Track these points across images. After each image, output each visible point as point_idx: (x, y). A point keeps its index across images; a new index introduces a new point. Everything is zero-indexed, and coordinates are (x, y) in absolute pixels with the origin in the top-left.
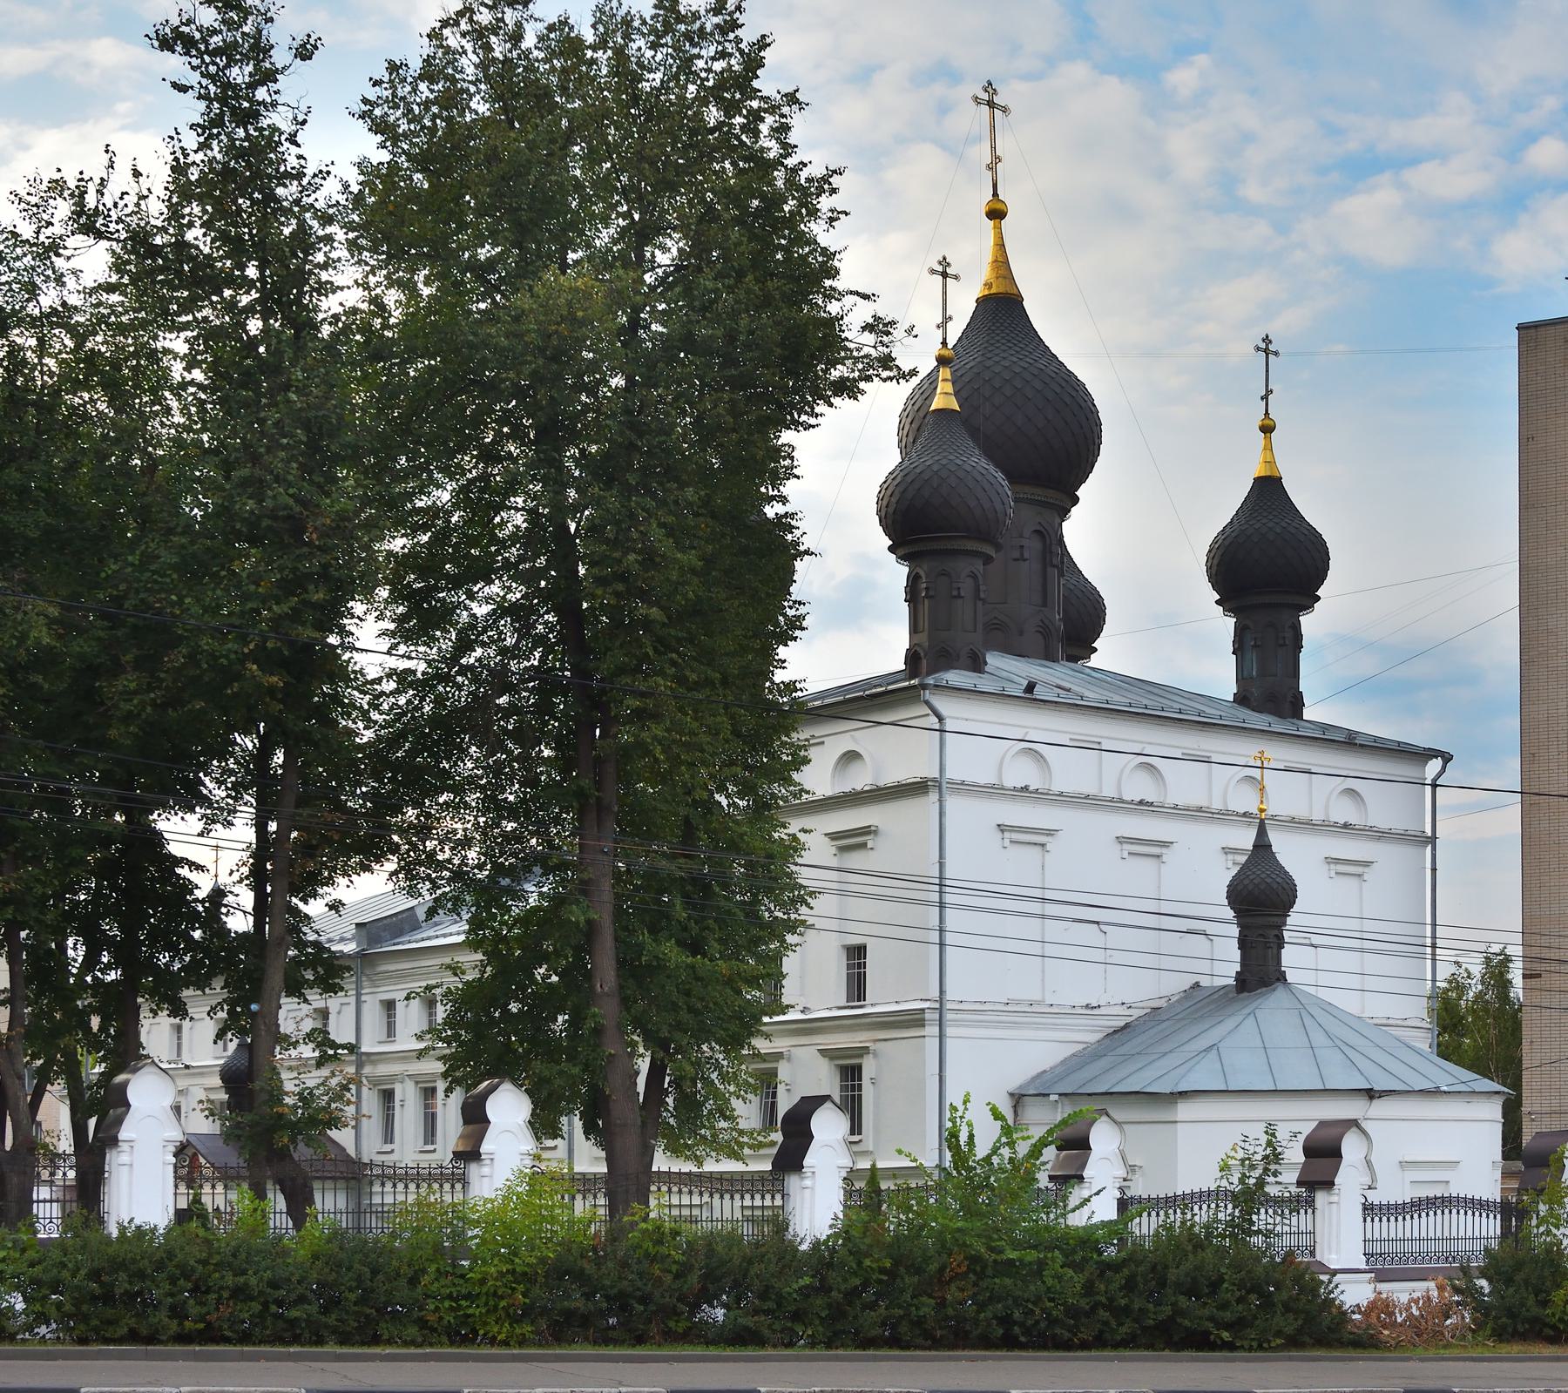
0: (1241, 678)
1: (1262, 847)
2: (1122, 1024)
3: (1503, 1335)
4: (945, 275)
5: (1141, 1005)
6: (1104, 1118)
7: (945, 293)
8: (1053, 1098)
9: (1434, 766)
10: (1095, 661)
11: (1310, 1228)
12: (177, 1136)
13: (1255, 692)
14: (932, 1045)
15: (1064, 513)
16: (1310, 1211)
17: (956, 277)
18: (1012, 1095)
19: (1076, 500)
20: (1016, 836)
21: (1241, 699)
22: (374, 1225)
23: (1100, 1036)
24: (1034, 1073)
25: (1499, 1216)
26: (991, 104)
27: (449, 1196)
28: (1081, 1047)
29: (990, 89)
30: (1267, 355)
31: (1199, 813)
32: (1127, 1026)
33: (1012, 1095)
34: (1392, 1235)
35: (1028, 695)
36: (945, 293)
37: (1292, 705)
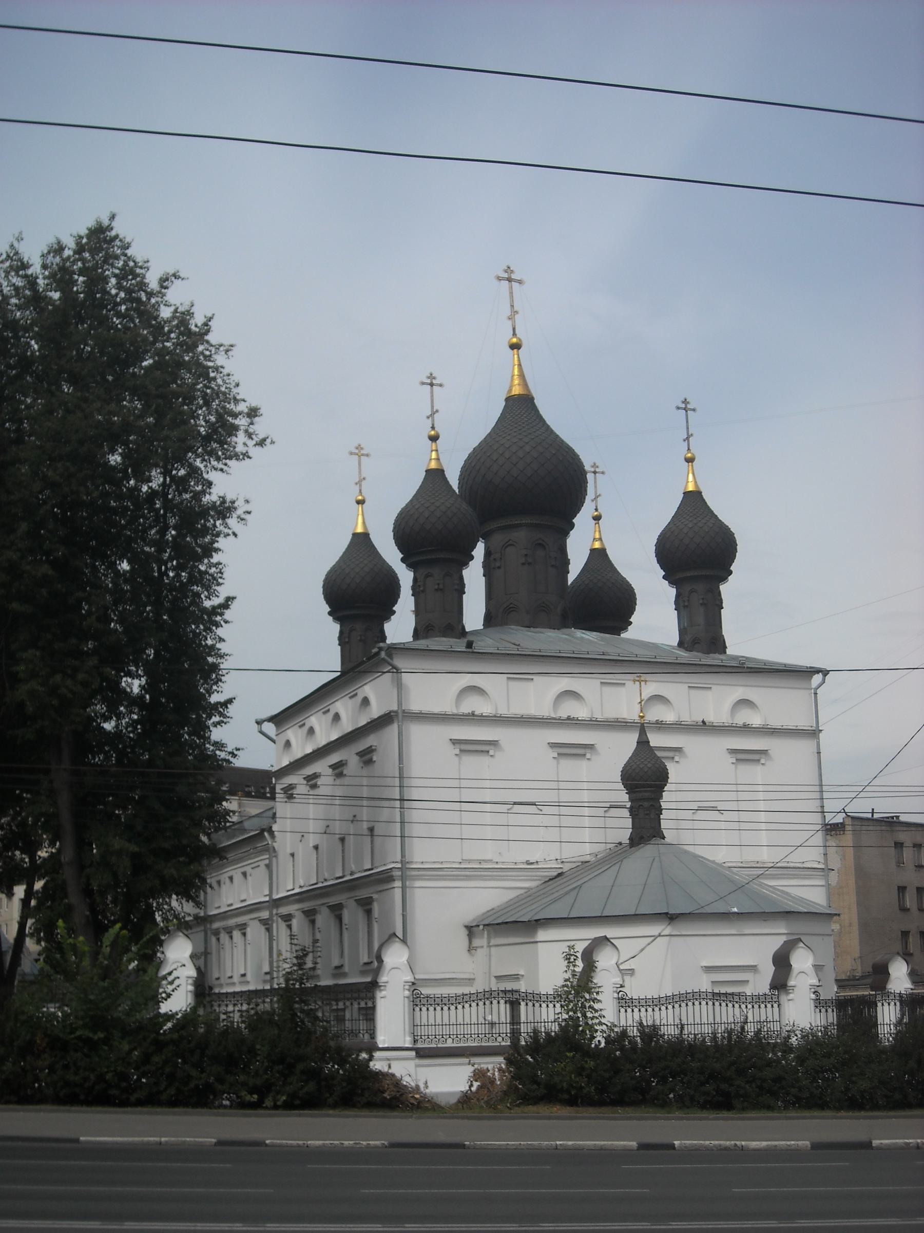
0: (682, 632)
1: (643, 743)
2: (555, 874)
3: (528, 1099)
4: (686, 409)
5: (574, 860)
6: (801, 945)
7: (432, 396)
8: (481, 927)
9: (817, 678)
10: (630, 634)
11: (776, 1017)
12: (409, 978)
13: (688, 638)
14: (398, 893)
15: (566, 533)
16: (776, 1005)
17: (694, 410)
18: (466, 927)
19: (572, 526)
20: (464, 747)
21: (681, 644)
22: (361, 1028)
23: (540, 882)
24: (489, 909)
25: (898, 1004)
26: (510, 280)
27: (766, 1013)
28: (522, 891)
29: (509, 271)
30: (686, 411)
31: (704, 727)
32: (560, 875)
33: (466, 927)
34: (467, 1020)
35: (470, 650)
36: (432, 396)
37: (717, 644)
